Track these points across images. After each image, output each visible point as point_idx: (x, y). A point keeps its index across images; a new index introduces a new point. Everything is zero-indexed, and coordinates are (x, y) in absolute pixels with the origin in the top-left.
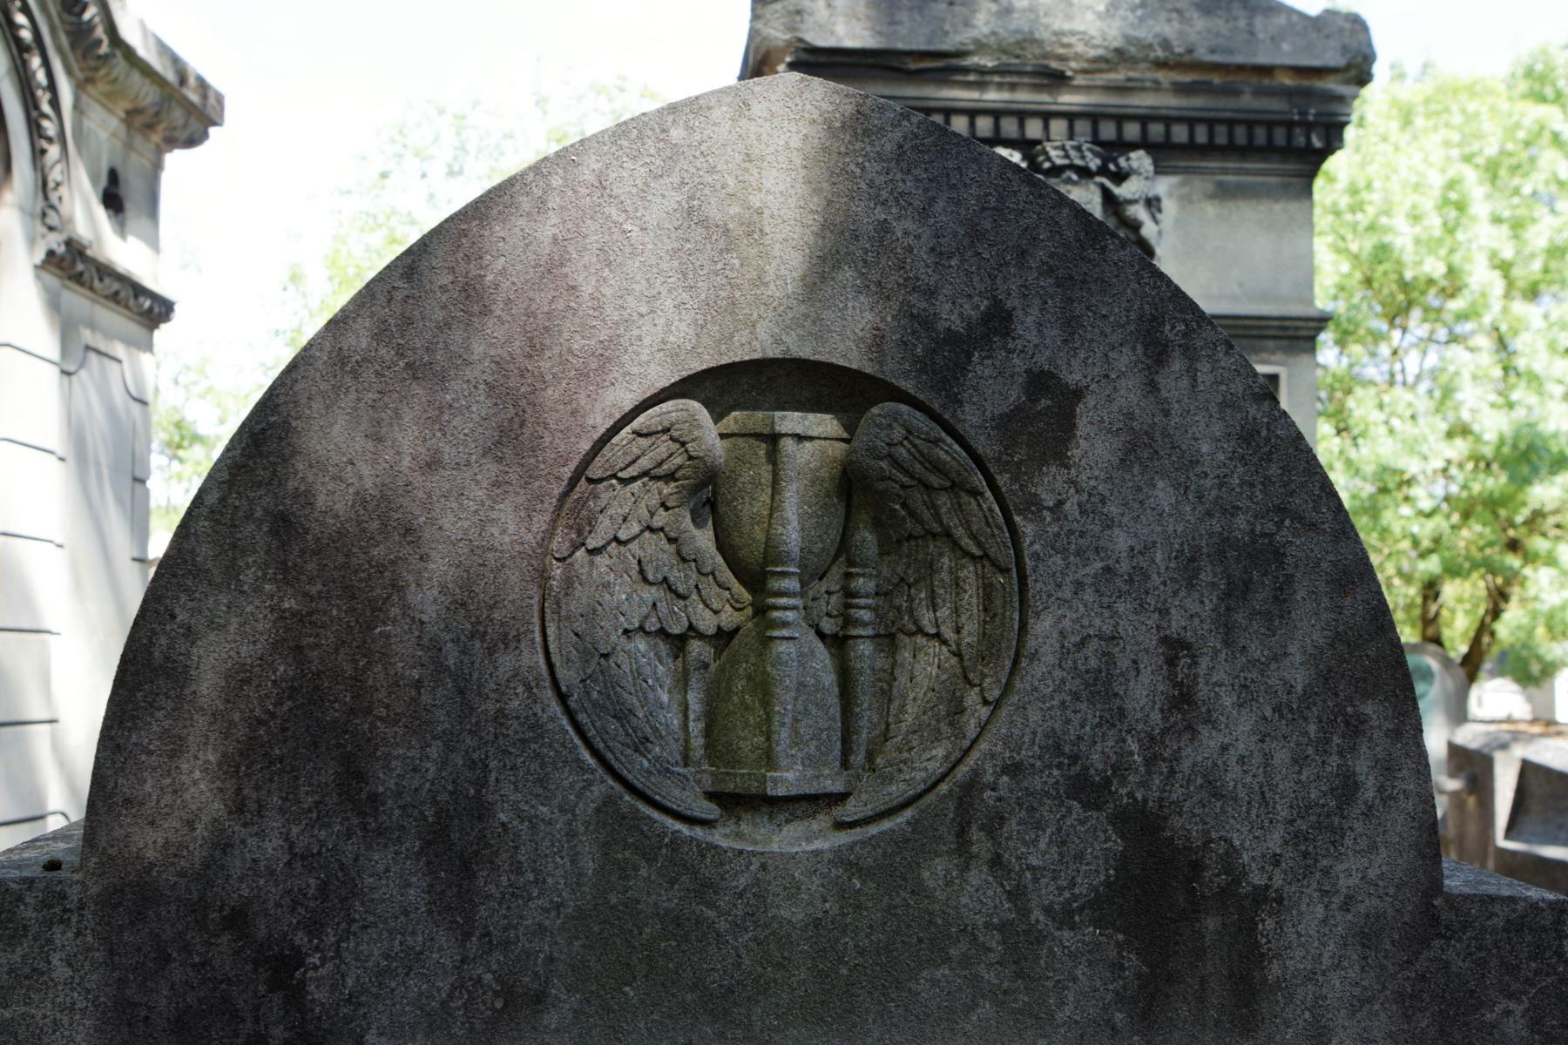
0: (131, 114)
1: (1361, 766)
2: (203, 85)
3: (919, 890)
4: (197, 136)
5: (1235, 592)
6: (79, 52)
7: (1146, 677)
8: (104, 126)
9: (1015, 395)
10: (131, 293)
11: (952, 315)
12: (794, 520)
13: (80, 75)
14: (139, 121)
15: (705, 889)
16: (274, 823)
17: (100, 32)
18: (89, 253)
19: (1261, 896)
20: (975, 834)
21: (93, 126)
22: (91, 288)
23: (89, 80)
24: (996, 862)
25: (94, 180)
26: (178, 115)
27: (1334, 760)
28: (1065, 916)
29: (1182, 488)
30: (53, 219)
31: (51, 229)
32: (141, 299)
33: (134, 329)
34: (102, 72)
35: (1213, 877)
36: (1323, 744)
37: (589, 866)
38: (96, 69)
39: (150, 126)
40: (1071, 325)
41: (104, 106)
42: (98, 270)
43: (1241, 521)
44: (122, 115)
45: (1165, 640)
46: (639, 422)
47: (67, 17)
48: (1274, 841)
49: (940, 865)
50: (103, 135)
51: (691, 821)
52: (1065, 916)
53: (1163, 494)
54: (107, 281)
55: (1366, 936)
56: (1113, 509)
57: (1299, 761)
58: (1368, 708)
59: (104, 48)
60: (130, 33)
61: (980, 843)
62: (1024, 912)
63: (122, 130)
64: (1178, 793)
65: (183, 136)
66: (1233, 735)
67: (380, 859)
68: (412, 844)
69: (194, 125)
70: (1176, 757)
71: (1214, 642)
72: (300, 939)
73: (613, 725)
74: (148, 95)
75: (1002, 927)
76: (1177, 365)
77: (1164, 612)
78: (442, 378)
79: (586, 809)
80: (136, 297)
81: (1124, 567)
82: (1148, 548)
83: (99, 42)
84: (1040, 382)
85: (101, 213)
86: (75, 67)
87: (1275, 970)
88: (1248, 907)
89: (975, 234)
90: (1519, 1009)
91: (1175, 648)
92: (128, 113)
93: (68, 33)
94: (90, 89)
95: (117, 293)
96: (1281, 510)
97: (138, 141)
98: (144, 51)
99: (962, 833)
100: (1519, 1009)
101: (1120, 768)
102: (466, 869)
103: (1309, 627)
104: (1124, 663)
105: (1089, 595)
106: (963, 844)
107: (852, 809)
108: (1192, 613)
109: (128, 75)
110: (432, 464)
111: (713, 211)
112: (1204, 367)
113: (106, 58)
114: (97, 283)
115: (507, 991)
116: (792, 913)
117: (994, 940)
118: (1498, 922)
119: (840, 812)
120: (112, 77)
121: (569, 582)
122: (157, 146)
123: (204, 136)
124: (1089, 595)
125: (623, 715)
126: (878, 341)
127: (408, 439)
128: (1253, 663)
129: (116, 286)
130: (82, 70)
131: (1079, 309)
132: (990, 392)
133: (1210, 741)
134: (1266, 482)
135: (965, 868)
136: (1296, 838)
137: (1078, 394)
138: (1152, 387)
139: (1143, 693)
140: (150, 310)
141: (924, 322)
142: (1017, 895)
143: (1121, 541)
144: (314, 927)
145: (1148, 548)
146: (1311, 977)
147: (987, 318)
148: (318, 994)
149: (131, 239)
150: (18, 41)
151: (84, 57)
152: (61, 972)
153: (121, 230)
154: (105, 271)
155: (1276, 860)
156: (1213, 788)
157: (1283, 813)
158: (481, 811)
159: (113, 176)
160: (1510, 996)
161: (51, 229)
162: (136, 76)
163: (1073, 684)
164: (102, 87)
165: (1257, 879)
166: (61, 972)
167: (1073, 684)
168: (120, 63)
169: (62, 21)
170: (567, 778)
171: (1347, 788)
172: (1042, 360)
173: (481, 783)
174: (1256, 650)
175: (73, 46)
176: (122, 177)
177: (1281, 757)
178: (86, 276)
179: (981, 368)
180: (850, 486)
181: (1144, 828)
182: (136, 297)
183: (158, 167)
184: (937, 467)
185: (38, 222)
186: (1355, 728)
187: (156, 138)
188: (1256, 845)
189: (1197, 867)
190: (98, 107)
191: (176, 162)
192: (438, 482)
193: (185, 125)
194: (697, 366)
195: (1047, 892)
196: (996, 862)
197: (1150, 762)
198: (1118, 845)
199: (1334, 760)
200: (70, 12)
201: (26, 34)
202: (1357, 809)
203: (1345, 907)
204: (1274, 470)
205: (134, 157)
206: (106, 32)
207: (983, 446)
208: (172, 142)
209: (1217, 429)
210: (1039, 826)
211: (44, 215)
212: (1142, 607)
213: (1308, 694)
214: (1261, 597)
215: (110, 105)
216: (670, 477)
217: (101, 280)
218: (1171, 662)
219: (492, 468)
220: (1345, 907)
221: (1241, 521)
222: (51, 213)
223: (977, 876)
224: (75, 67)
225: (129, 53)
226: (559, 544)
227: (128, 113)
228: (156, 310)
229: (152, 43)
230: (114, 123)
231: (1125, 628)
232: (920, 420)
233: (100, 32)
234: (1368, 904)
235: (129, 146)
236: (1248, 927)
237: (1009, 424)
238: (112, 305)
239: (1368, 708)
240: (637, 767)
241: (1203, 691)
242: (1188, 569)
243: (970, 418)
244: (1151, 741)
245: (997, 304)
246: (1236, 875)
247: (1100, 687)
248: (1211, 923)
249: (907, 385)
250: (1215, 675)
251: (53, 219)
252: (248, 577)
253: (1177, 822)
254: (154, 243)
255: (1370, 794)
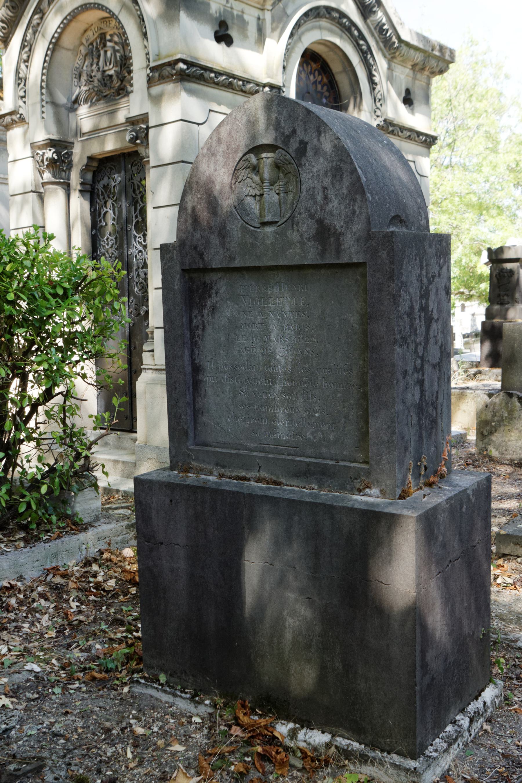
0: (414, 66)
1: (356, 208)
2: (442, 48)
3: (287, 237)
4: (443, 69)
5: (334, 176)
6: (387, 48)
7: (320, 194)
8: (403, 74)
9: (297, 145)
10: (416, 135)
11: (287, 132)
12: (267, 174)
13: (389, 57)
14: (417, 68)
15: (256, 238)
16: (199, 232)
17: (394, 39)
18: (395, 122)
19: (340, 234)
20: (295, 226)
21: (398, 74)
22: (399, 136)
23: (393, 58)
24: (298, 231)
25: (399, 95)
26: (433, 63)
27: (351, 207)
28: (309, 240)
29: (324, 158)
30: (378, 113)
31: (378, 116)
32: (421, 137)
33: (425, 150)
34: (397, 54)
35: (332, 231)
36: (349, 204)
37: (240, 236)
38: (395, 53)
39: (423, 69)
40: (306, 130)
41: (402, 65)
42: (400, 129)
43: (334, 163)
44: (410, 67)
45: (323, 187)
46: (243, 159)
47: (381, 36)
48: (342, 223)
49: (290, 232)
50: (403, 77)
51: (255, 227)
52: (309, 240)
53: (322, 160)
54: (405, 132)
55: (358, 240)
56: (313, 164)
57: (346, 208)
58: (357, 196)
59: (396, 45)
60: (405, 36)
61: (295, 228)
62: (303, 239)
63: (411, 73)
64: (326, 215)
65: (438, 70)
66: (334, 205)
67: (213, 237)
68: (216, 234)
69: (441, 65)
70: (325, 209)
71: (331, 187)
72: (203, 250)
73: (243, 212)
74: (418, 57)
75: (299, 242)
76: (323, 135)
77: (322, 182)
78: (216, 155)
79: (239, 226)
80: (418, 136)
81: (316, 174)
82: (320, 170)
83: (394, 43)
84: (302, 142)
85: (402, 107)
86: (387, 54)
87: (343, 247)
88: (338, 236)
89: (290, 116)
90: (385, 252)
91: (325, 188)
92: (413, 66)
93: (383, 42)
94: (395, 60)
95: (410, 136)
96: (341, 160)
97: (419, 76)
98: (414, 42)
99: (292, 226)
100: (385, 252)
101: (316, 212)
102: (224, 238)
103: (347, 182)
104: (316, 192)
105: (310, 180)
106: (293, 229)
107: (279, 223)
108: (327, 182)
109: (408, 52)
110: (216, 170)
111: (251, 120)
112: (327, 134)
113: (398, 48)
114: (400, 133)
115: (230, 258)
116: (268, 242)
117: (298, 245)
118: (381, 236)
119: (278, 224)
120: (402, 54)
121: (235, 188)
122: (428, 76)
123: (447, 68)
124: (310, 180)
125: (245, 210)
126: (276, 139)
127: (212, 166)
128: (338, 190)
129: (408, 134)
130: (390, 54)
131: (307, 127)
132: (294, 145)
133: (331, 205)
134: (338, 155)
135: (293, 232)
136: (346, 222)
137: (307, 143)
138: (319, 140)
139: (319, 197)
140: (426, 140)
141: (283, 134)
142: (301, 236)
143: (315, 170)
144: (205, 248)
145: (320, 170)
146: (349, 248)
147: (292, 132)
148: (206, 259)
149: (417, 115)
150: (362, 50)
151: (390, 50)
152: (175, 257)
153: (412, 112)
154: (403, 129)
155: (342, 227)
156: (332, 215)
157: (343, 218)
158: (225, 228)
159: (408, 91)
160: (384, 250)
161: (378, 116)
162: (412, 52)
163: (309, 197)
164: (399, 59)
165: (339, 231)
166: (175, 257)
167: (309, 197)
168: (404, 48)
169: (380, 38)
170: (236, 221)
171: (354, 212)
172: (301, 138)
173: (225, 223)
174: (338, 188)
175: (385, 46)
176: (411, 92)
177: (343, 207)
178: (395, 132)
179: (292, 141)
180: (277, 166)
181: (320, 222)
182: (418, 136)
183: (429, 84)
184: (287, 160)
185: (373, 114)
186: (355, 200)
187: (426, 73)
188: (339, 224)
189: (329, 229)
190: (399, 66)
191: (436, 81)
192: (216, 173)
193: (437, 66)
194: (250, 147)
195: (306, 236)
196: (298, 231)
197: (321, 210)
198: (316, 226)
199: (351, 207)
200: (382, 35)
201: (364, 47)
202: (356, 216)
203: (354, 235)
204: (339, 153)
205: (417, 82)
206: (396, 38)
207: (293, 155)
208: (433, 73)
209: (330, 146)
210: (304, 224)
211: (375, 112)
212: (319, 182)
213: (346, 195)
214: (338, 177)
215: (404, 65)
216: (249, 168)
217: (402, 132)
218: (324, 191)
219: (223, 170)
220: (354, 235)
221: (334, 163)
222: (377, 110)
223: (295, 233)
224: (387, 54)
225: (407, 44)
226: (233, 182)
227: (413, 66)
228: (428, 140)
229: (415, 38)
230: (407, 71)
231: (316, 186)
232: (284, 152)
233: (394, 39)
234: (358, 234)
235: (414, 78)
236: (338, 239)
237: (297, 151)
238: (409, 141)
239: (357, 196)
240: (247, 219)
241: (329, 196)
242: (326, 173)
243: (291, 150)
244: (321, 207)
245: (294, 128)
246: (335, 229)
247: (313, 197)
248: (332, 239)
249: (281, 146)
250: (331, 193)
251: (378, 113)
252: (193, 192)
253: (326, 221)
254: (428, 115)
255: (358, 213)
